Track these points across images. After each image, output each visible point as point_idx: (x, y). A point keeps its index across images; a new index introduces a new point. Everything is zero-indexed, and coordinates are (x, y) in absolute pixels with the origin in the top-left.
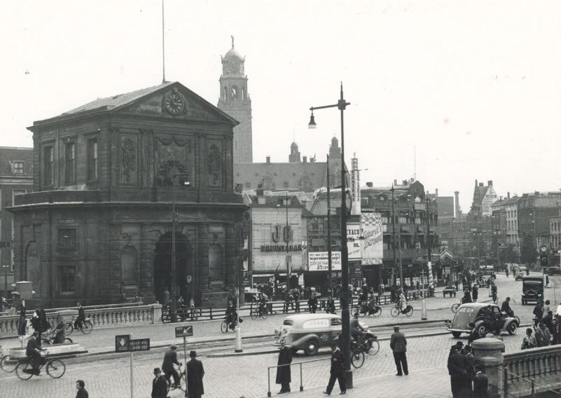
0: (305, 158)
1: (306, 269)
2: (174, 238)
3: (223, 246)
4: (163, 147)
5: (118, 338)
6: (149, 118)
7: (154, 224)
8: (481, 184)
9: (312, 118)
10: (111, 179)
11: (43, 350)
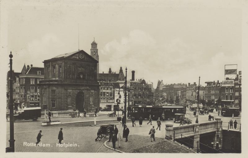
8: (160, 81)
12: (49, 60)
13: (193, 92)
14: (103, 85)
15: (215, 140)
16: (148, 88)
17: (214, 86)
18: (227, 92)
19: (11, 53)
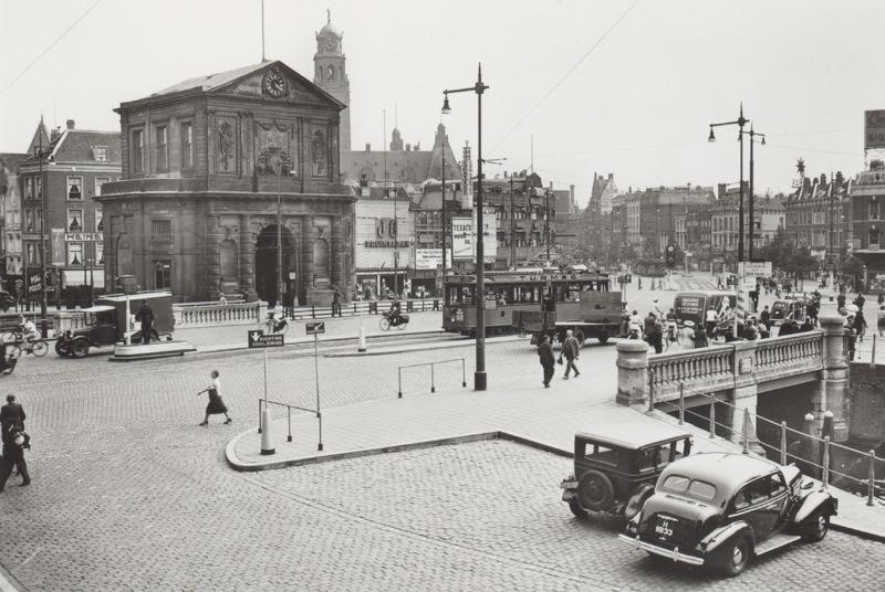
0: (408, 146)
1: (413, 267)
2: (279, 232)
3: (329, 241)
4: (263, 132)
5: (251, 333)
6: (249, 100)
7: (256, 216)
8: (601, 178)
9: (446, 102)
10: (207, 166)
11: (690, 287)
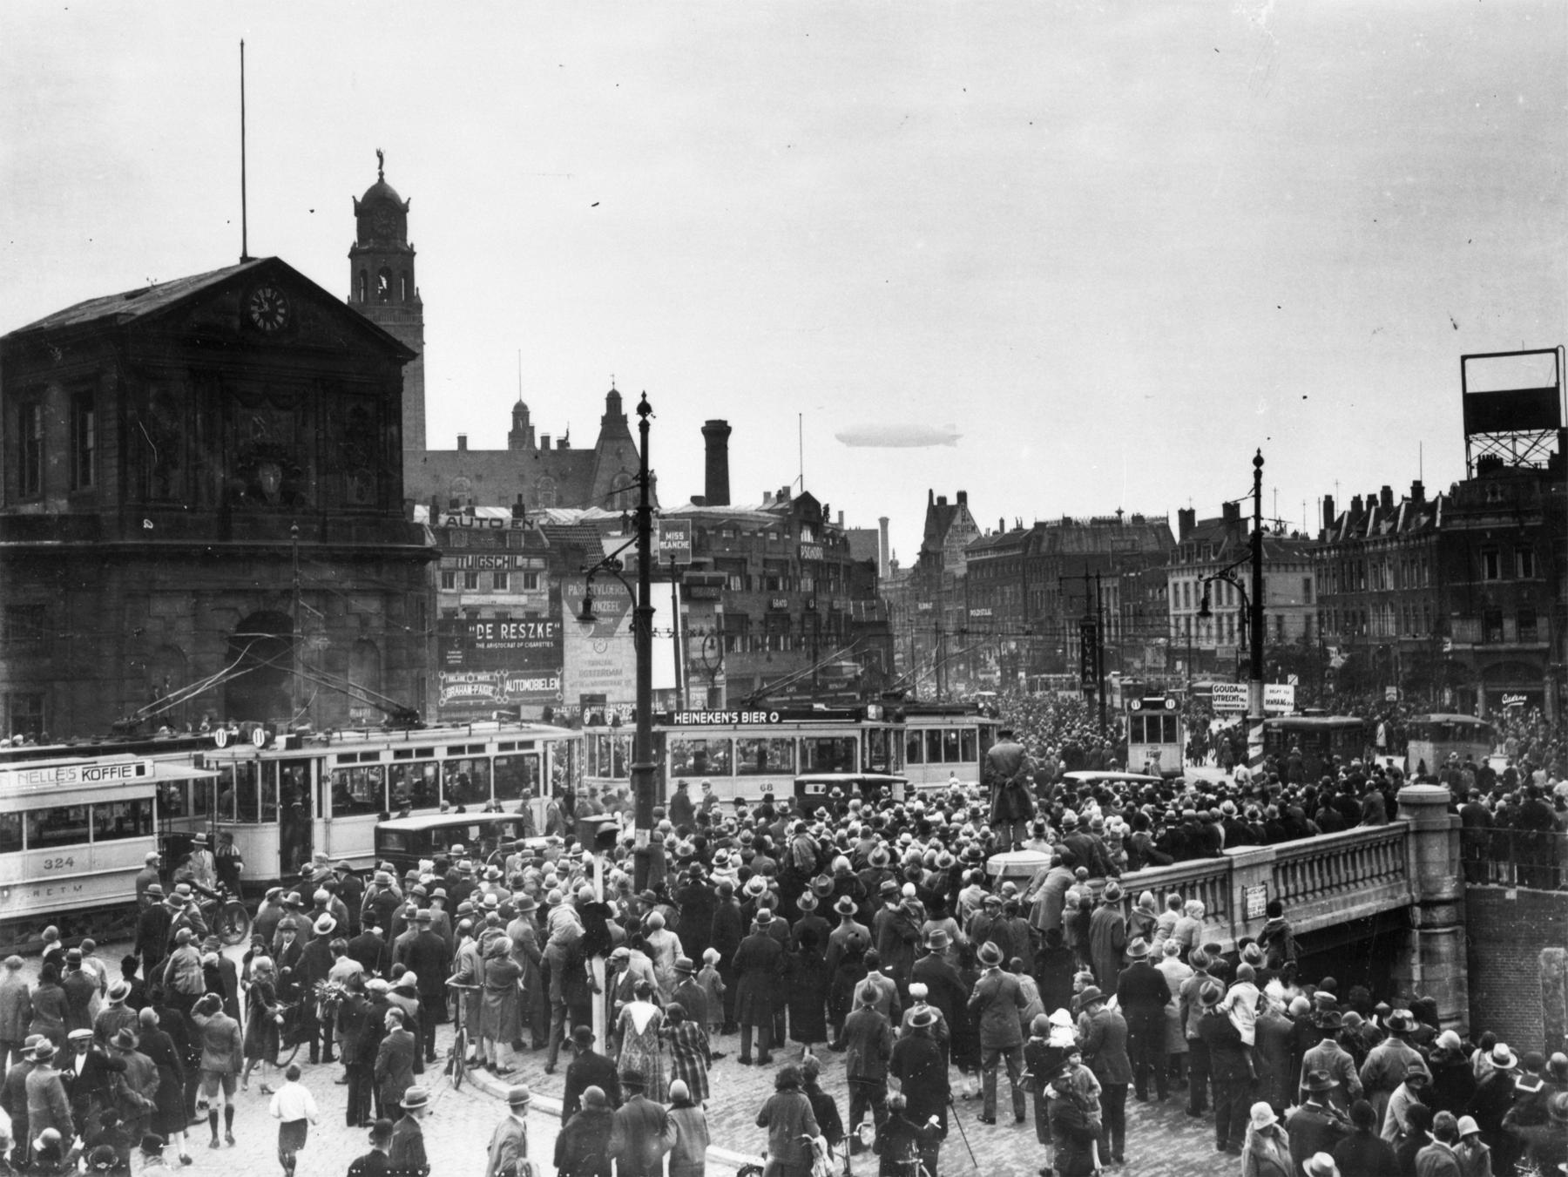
0: (546, 440)
8: (942, 500)
12: (400, 467)
13: (1207, 585)
14: (460, 553)
15: (1411, 981)
16: (849, 560)
17: (1385, 527)
18: (1493, 575)
19: (644, 395)
